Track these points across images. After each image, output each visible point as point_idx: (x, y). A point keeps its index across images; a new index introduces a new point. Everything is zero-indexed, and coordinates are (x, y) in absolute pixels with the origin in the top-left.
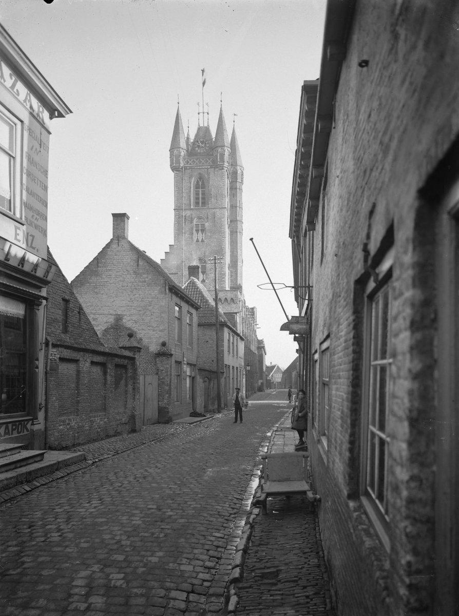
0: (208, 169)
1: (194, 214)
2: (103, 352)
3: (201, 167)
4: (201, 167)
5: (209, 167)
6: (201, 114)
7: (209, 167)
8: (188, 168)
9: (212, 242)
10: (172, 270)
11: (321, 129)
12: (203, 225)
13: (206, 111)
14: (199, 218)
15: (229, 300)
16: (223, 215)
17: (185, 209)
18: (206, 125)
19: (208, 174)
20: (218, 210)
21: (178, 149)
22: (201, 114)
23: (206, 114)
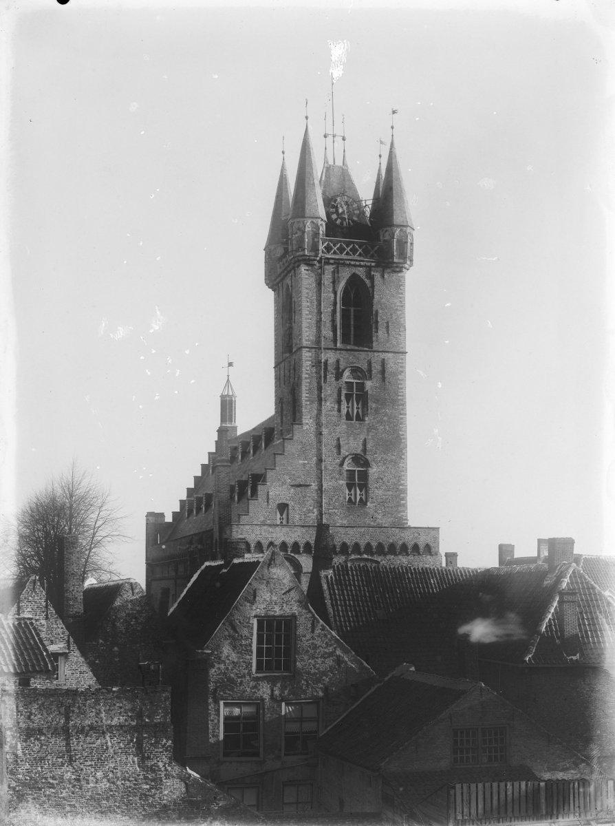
0: (370, 267)
1: (345, 359)
2: (219, 532)
3: (357, 263)
4: (357, 263)
5: (373, 264)
6: (330, 138)
7: (373, 264)
8: (332, 261)
9: (378, 422)
10: (299, 477)
11: (365, 240)
12: (361, 387)
13: (339, 132)
14: (355, 371)
15: (422, 547)
16: (401, 367)
17: (325, 349)
18: (339, 163)
19: (372, 278)
20: (390, 355)
21: (315, 221)
22: (330, 138)
23: (338, 139)
